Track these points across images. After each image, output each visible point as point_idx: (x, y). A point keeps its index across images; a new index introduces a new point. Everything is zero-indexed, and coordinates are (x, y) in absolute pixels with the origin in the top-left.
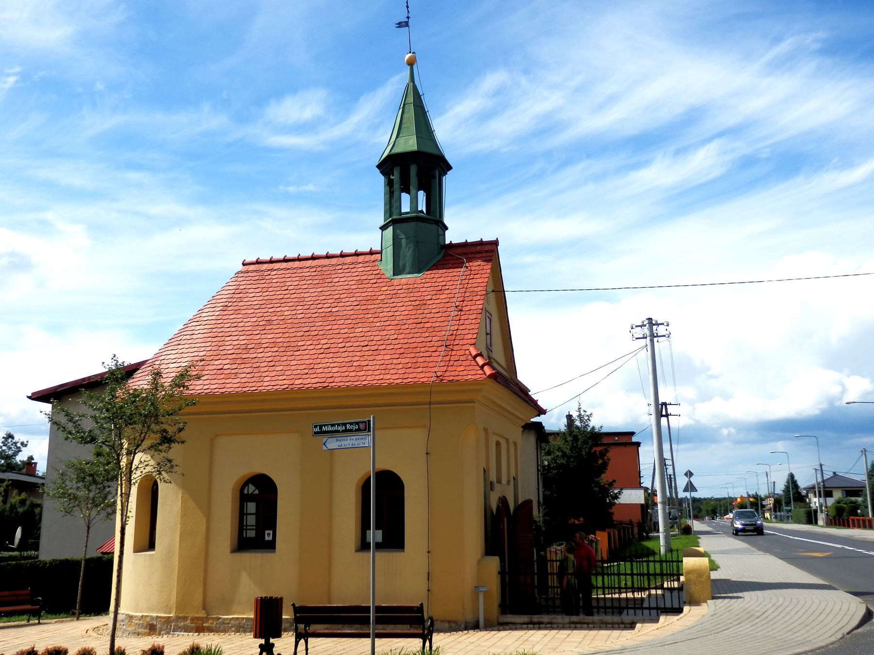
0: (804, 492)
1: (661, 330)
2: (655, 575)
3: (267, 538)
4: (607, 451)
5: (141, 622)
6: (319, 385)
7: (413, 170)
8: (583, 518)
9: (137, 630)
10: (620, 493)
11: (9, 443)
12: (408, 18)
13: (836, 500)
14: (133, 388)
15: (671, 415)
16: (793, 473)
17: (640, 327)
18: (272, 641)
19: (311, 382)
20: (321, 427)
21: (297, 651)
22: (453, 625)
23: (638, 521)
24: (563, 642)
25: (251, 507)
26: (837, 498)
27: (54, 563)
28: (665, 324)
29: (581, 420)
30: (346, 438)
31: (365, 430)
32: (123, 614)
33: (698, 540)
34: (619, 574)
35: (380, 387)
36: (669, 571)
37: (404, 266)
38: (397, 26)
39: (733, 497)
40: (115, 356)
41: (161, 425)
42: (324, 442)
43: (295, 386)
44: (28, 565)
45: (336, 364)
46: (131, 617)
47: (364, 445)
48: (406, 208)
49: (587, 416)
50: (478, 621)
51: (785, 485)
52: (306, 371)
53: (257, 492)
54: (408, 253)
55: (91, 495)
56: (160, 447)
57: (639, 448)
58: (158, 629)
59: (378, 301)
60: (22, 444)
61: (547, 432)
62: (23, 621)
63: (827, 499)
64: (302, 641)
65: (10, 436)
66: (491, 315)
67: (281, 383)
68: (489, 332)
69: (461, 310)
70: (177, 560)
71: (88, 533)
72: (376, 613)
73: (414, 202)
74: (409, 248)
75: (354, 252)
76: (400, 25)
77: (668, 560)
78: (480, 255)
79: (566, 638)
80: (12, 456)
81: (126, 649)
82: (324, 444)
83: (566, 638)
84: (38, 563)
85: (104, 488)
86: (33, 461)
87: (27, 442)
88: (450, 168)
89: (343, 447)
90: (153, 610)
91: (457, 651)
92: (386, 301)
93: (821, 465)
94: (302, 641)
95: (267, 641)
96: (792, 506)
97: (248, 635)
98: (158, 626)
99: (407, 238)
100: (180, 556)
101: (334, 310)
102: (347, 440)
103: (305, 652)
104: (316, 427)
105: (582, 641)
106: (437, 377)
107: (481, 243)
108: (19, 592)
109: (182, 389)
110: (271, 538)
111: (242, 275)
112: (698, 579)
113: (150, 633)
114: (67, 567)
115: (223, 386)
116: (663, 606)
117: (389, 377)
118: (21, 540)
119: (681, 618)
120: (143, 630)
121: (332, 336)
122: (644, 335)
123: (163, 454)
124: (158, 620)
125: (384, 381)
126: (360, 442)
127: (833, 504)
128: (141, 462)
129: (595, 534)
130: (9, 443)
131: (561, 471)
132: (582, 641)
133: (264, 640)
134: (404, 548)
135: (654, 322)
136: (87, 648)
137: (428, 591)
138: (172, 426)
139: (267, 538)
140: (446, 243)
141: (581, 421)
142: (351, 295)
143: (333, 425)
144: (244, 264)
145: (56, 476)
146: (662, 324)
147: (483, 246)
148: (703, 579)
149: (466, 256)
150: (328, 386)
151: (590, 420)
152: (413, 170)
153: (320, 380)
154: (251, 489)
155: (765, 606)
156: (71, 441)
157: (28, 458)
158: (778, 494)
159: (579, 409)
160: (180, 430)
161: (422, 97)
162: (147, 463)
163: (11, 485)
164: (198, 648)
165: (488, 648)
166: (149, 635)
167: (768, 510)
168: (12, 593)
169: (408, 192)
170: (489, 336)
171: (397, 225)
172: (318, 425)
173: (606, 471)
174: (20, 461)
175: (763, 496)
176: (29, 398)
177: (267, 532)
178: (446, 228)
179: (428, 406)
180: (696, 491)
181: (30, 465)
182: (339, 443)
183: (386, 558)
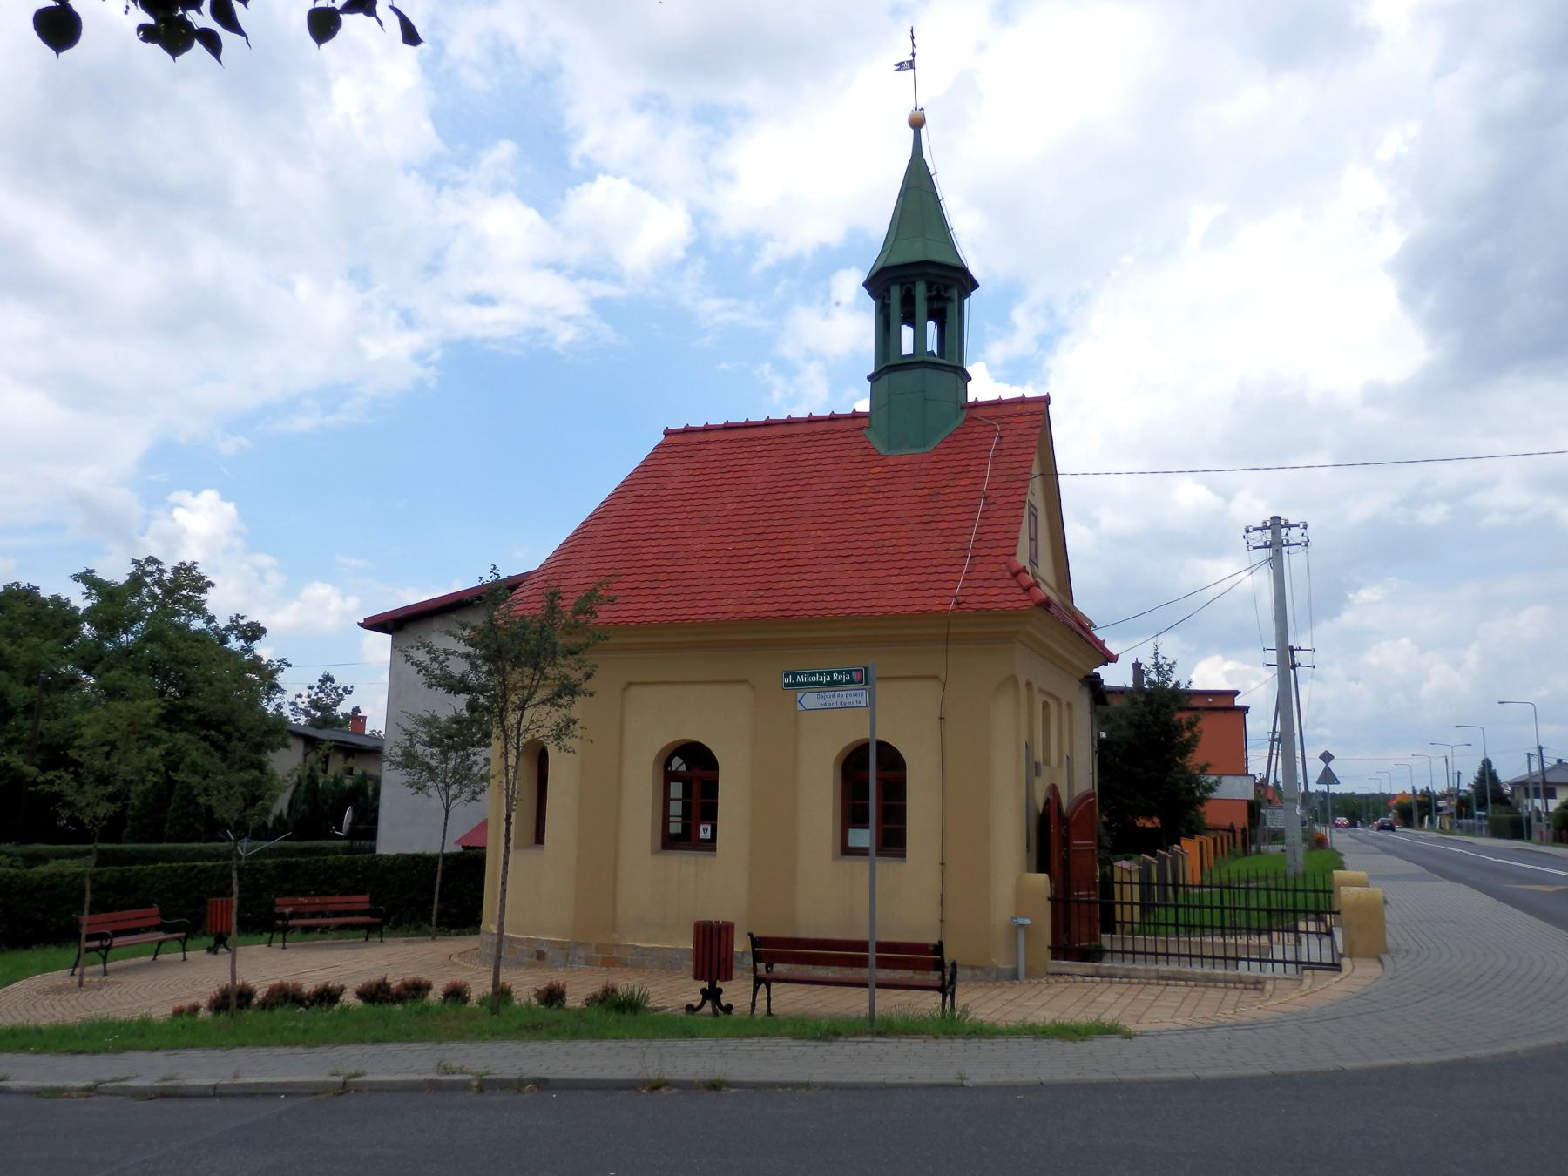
0: (1508, 790)
1: (1294, 535)
2: (1282, 911)
3: (703, 835)
4: (1198, 719)
6: (664, 618)
7: (920, 291)
8: (1158, 817)
10: (1217, 783)
11: (327, 688)
12: (913, 55)
13: (1562, 803)
14: (520, 613)
15: (1299, 666)
16: (1490, 759)
17: (1260, 531)
18: (719, 984)
20: (794, 677)
21: (757, 999)
23: (1242, 826)
24: (1150, 1006)
25: (676, 789)
26: (1563, 800)
28: (1301, 525)
29: (1158, 671)
30: (831, 694)
31: (861, 682)
33: (1341, 858)
34: (1201, 907)
38: (897, 68)
39: (1377, 792)
40: (495, 568)
41: (560, 669)
42: (798, 699)
43: (745, 615)
45: (804, 583)
47: (859, 705)
48: (907, 346)
49: (1168, 665)
50: (1016, 970)
51: (1475, 778)
53: (683, 768)
55: (451, 765)
56: (559, 701)
57: (1246, 715)
59: (866, 489)
60: (345, 689)
61: (1106, 689)
62: (359, 937)
63: (1549, 800)
64: (763, 987)
65: (328, 678)
66: (1037, 511)
67: (723, 609)
68: (1033, 537)
71: (446, 818)
72: (877, 952)
73: (919, 339)
76: (900, 66)
77: (1279, 887)
79: (1154, 1001)
80: (331, 706)
81: (568, 984)
82: (800, 702)
83: (1154, 1001)
85: (469, 755)
86: (359, 714)
87: (352, 687)
88: (975, 285)
89: (827, 707)
91: (989, 1012)
92: (877, 489)
93: (1540, 749)
94: (763, 987)
95: (712, 984)
96: (1490, 808)
97: (678, 974)
102: (833, 696)
103: (766, 1002)
104: (787, 676)
105: (1180, 1006)
106: (958, 604)
109: (588, 615)
110: (708, 836)
111: (665, 449)
114: (418, 865)
115: (640, 613)
116: (1305, 959)
117: (884, 602)
118: (353, 824)
119: (1341, 980)
121: (798, 541)
122: (1266, 542)
123: (563, 711)
125: (877, 609)
126: (853, 699)
127: (1557, 809)
128: (533, 721)
129: (1179, 844)
130: (327, 688)
131: (62, 752)
132: (1180, 1006)
133: (707, 983)
134: (715, 850)
135: (1283, 523)
136: (458, 982)
137: (942, 921)
138: (576, 670)
139: (703, 835)
141: (1159, 673)
142: (826, 479)
145: (401, 737)
146: (1297, 526)
147: (1026, 406)
149: (1001, 421)
151: (1171, 672)
152: (920, 291)
153: (781, 607)
154: (677, 764)
155: (1478, 967)
156: (436, 690)
157: (353, 710)
158: (1465, 791)
159: (1156, 654)
160: (588, 676)
161: (934, 177)
162: (540, 723)
163: (335, 747)
164: (613, 990)
165: (1037, 1010)
167: (1447, 815)
169: (911, 323)
170: (1033, 542)
173: (1196, 749)
174: (342, 714)
175: (1437, 794)
176: (361, 625)
177: (702, 827)
178: (969, 378)
180: (1338, 783)
181: (356, 718)
182: (822, 701)
183: (887, 868)
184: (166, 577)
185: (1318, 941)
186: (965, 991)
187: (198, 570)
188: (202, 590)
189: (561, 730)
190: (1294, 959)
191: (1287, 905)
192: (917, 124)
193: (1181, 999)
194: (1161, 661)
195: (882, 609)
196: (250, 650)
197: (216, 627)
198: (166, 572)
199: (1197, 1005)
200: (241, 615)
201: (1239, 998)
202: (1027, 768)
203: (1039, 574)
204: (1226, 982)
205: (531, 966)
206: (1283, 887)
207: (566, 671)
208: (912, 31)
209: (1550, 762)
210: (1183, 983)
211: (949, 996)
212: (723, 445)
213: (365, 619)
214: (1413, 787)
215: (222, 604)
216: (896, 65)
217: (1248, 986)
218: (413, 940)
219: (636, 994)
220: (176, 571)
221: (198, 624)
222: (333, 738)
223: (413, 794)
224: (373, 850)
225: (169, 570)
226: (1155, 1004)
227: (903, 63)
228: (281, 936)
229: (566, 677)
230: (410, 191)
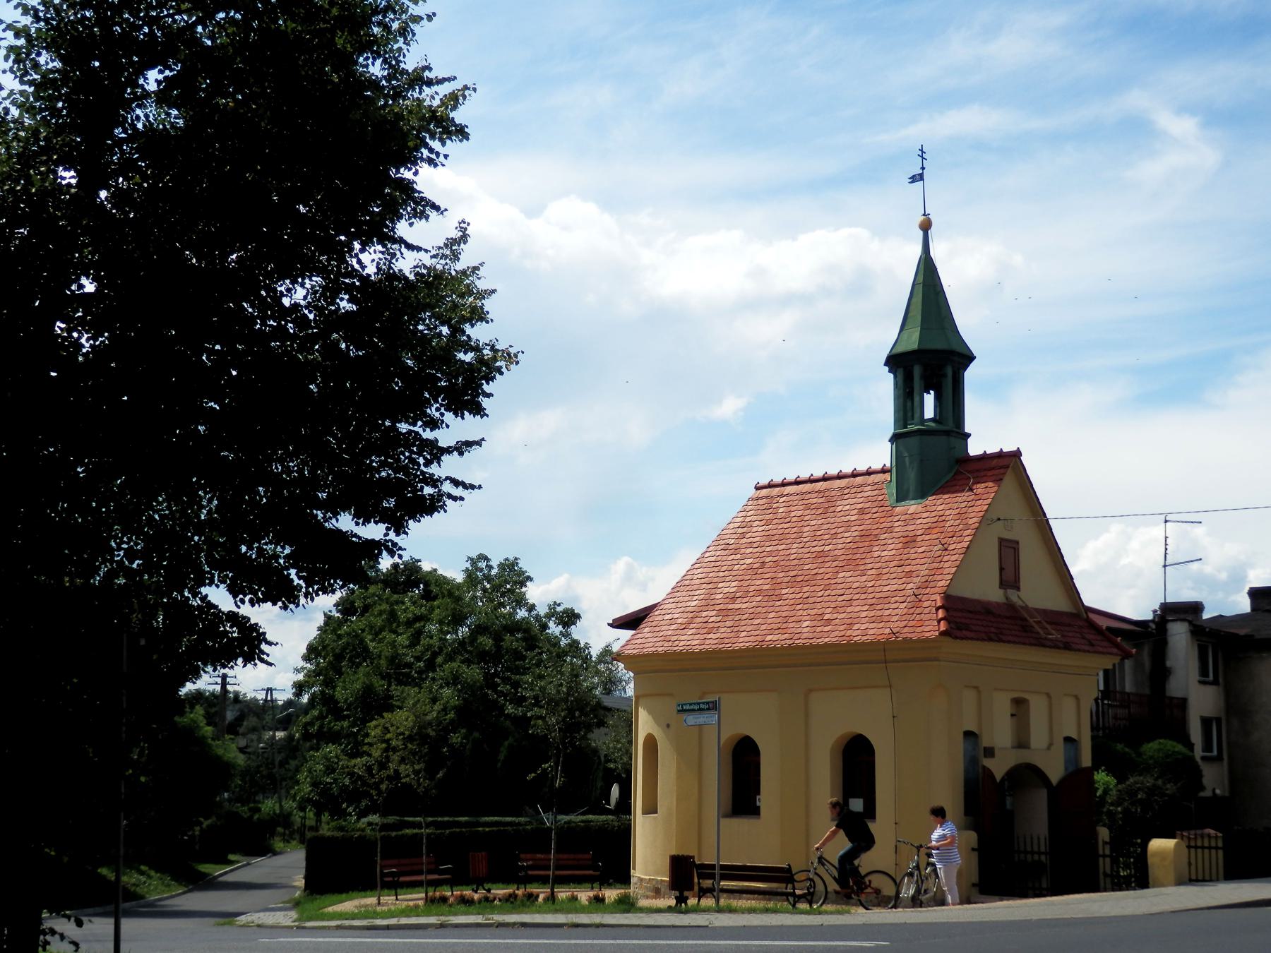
7: (917, 371)
12: (923, 168)
20: (682, 707)
27: (566, 826)
36: (1200, 855)
37: (908, 491)
38: (910, 180)
44: (597, 828)
46: (641, 880)
52: (779, 625)
54: (912, 475)
69: (946, 550)
74: (913, 468)
75: (881, 467)
78: (990, 473)
84: (606, 826)
90: (658, 874)
98: (662, 890)
99: (911, 456)
101: (827, 548)
107: (1000, 455)
108: (581, 856)
124: (663, 883)
137: (896, 864)
143: (691, 704)
144: (757, 488)
152: (917, 371)
168: (572, 856)
171: (900, 441)
184: (494, 572)
187: (520, 566)
188: (523, 584)
192: (926, 226)
196: (567, 635)
197: (537, 615)
198: (493, 568)
200: (558, 602)
213: (613, 620)
215: (539, 594)
216: (910, 179)
220: (501, 566)
221: (522, 614)
225: (495, 566)
228: (523, 886)
230: (210, 739)
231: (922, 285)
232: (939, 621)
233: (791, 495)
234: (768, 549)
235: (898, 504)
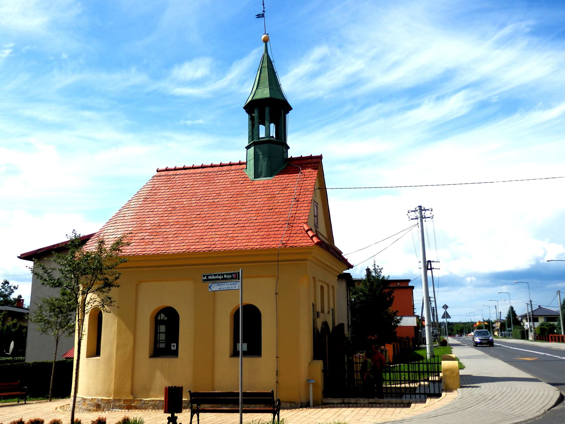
1: (427, 214)
2: (423, 372)
3: (172, 348)
4: (392, 292)
5: (91, 403)
7: (267, 110)
9: (88, 407)
10: (401, 319)
11: (6, 287)
12: (264, 11)
15: (434, 269)
16: (513, 306)
17: (414, 212)
18: (176, 415)
19: (201, 247)
20: (207, 276)
22: (293, 405)
28: (430, 210)
29: (375, 272)
30: (223, 284)
31: (236, 278)
32: (79, 397)
33: (451, 349)
34: (400, 372)
35: (246, 250)
37: (261, 172)
38: (257, 17)
40: (74, 231)
41: (104, 275)
46: (84, 400)
47: (235, 288)
48: (262, 134)
49: (380, 269)
50: (309, 403)
53: (166, 318)
56: (104, 290)
58: (102, 407)
59: (244, 195)
60: (14, 287)
61: (353, 280)
62: (15, 402)
63: (535, 323)
65: (7, 282)
66: (317, 204)
67: (181, 248)
68: (316, 215)
69: (298, 201)
70: (115, 362)
71: (57, 345)
73: (268, 131)
74: (265, 161)
75: (229, 163)
76: (259, 16)
77: (432, 362)
79: (366, 413)
80: (8, 295)
81: (82, 420)
82: (210, 287)
83: (366, 413)
85: (67, 316)
86: (21, 299)
87: (18, 286)
89: (222, 289)
90: (99, 395)
92: (249, 195)
93: (531, 301)
94: (195, 415)
95: (173, 415)
96: (512, 328)
98: (102, 405)
99: (263, 154)
100: (116, 360)
103: (197, 422)
104: (204, 276)
105: (376, 415)
106: (283, 244)
107: (311, 157)
109: (117, 252)
110: (175, 348)
111: (156, 178)
112: (451, 375)
113: (97, 409)
114: (43, 367)
116: (428, 392)
117: (251, 244)
120: (92, 408)
123: (105, 294)
124: (103, 401)
126: (233, 286)
128: (91, 299)
129: (385, 346)
130: (6, 287)
132: (376, 415)
133: (171, 414)
134: (178, 355)
135: (423, 209)
136: (56, 419)
137: (277, 382)
138: (111, 276)
139: (172, 348)
140: (288, 157)
141: (376, 273)
144: (158, 171)
145: (36, 308)
146: (428, 210)
148: (455, 375)
150: (212, 250)
151: (381, 272)
152: (267, 110)
154: (163, 316)
156: (46, 286)
157: (18, 296)
158: (503, 320)
159: (375, 264)
160: (117, 278)
162: (95, 300)
165: (316, 419)
166: (97, 411)
167: (497, 330)
169: (264, 125)
170: (316, 217)
172: (206, 275)
174: (13, 298)
175: (493, 321)
176: (19, 257)
177: (172, 344)
178: (289, 148)
179: (277, 263)
180: (450, 318)
182: (219, 287)
185: (433, 384)
186: (338, 410)
189: (104, 303)
190: (424, 392)
191: (416, 370)
193: (377, 412)
194: (377, 267)
195: (250, 247)
199: (383, 414)
201: (401, 410)
202: (314, 315)
203: (319, 231)
204: (396, 404)
205: (94, 411)
206: (434, 362)
207: (106, 276)
208: (263, 2)
209: (535, 307)
210: (379, 405)
211: (276, 415)
212: (182, 176)
214: (483, 319)
216: (257, 16)
217: (405, 405)
218: (57, 401)
219: (138, 421)
222: (7, 309)
223: (41, 334)
224: (24, 360)
226: (366, 414)
227: (260, 14)
229: (107, 279)
231: (267, 67)
232: (312, 238)
233: (182, 174)
234: (175, 201)
235: (255, 179)
